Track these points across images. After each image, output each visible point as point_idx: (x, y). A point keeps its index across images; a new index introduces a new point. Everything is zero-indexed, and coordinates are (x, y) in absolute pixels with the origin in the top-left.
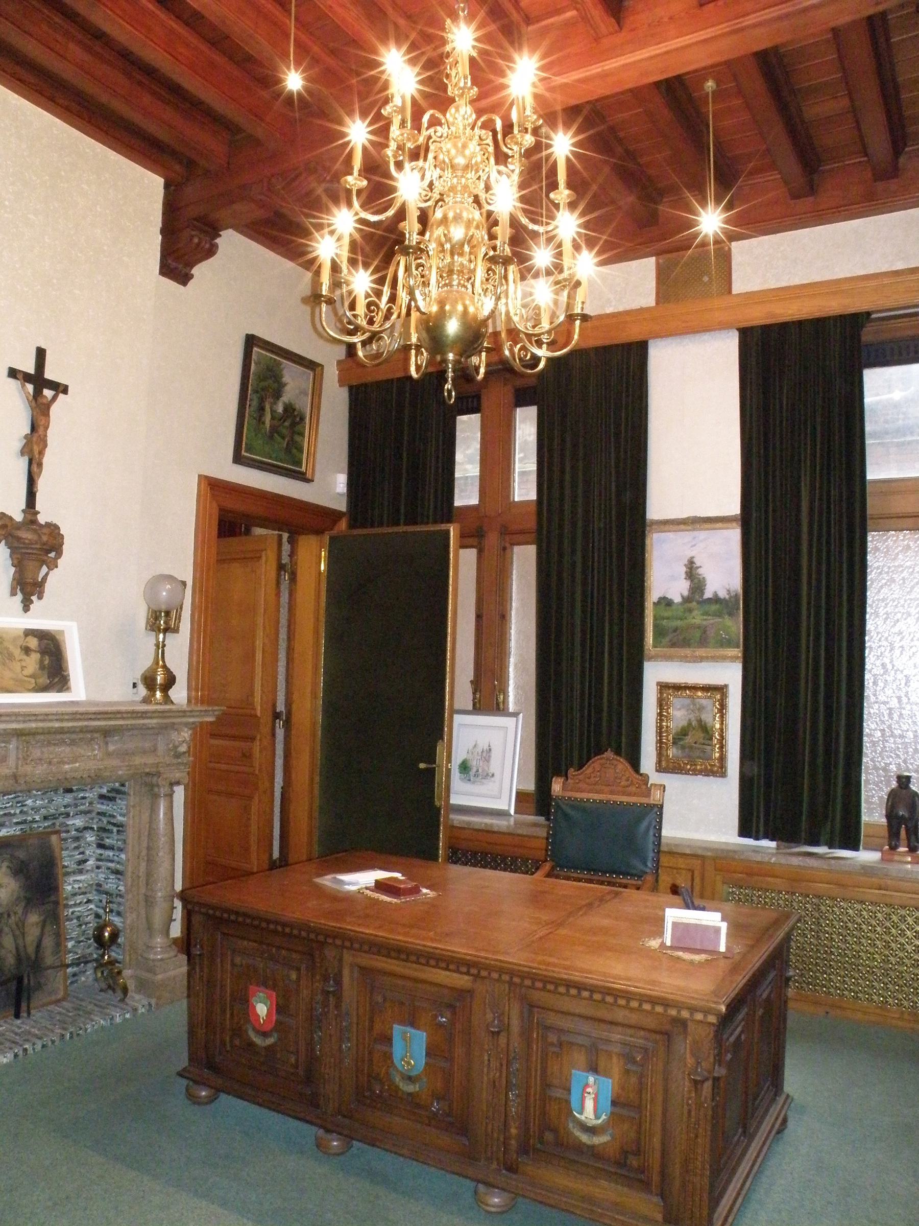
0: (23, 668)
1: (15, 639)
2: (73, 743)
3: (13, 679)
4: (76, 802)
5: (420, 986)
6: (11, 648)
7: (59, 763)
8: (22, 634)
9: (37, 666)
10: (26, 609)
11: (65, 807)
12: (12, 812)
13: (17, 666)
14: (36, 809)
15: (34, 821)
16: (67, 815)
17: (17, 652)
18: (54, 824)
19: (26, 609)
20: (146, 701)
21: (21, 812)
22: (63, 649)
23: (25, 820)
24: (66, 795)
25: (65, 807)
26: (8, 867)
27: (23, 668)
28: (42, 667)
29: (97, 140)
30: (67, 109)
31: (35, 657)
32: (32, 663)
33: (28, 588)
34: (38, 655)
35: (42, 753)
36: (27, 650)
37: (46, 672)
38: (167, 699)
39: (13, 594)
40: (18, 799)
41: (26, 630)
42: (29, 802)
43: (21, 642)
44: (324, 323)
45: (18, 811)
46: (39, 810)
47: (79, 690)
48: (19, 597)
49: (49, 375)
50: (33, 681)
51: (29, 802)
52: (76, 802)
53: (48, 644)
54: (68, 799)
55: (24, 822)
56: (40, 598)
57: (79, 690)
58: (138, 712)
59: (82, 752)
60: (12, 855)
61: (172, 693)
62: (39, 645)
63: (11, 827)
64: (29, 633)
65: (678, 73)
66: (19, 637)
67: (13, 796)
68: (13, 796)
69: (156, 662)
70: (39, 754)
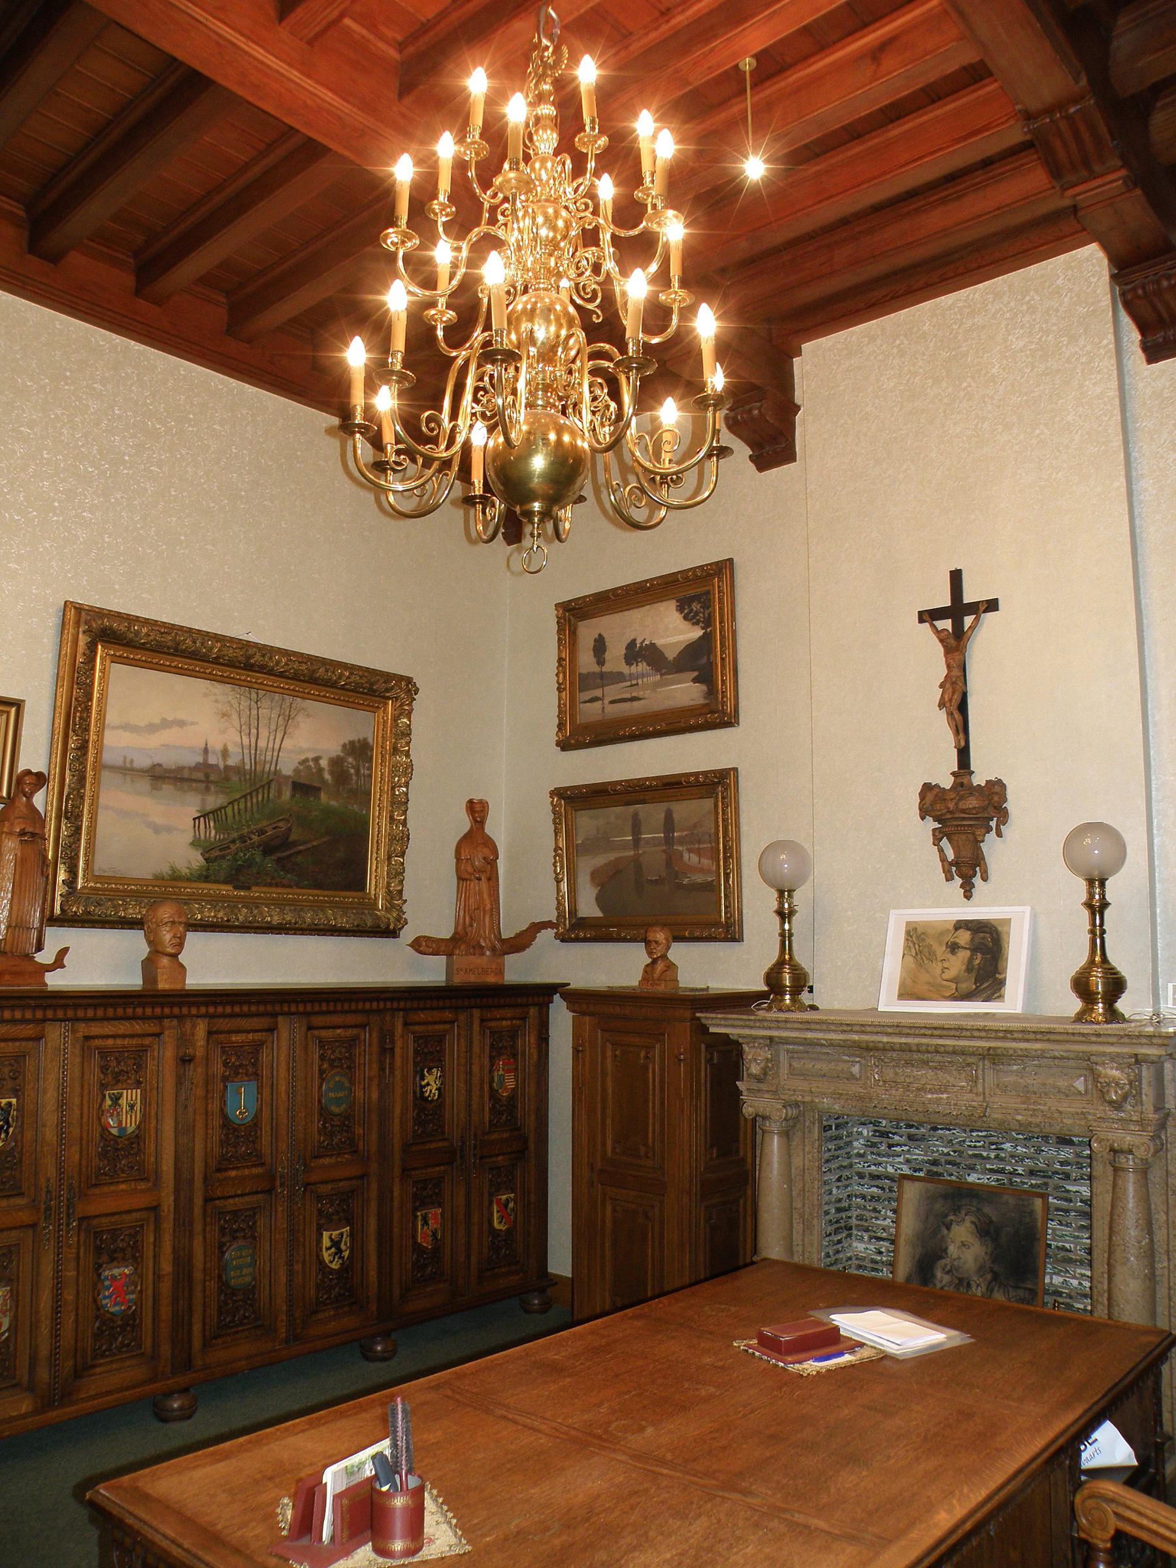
0: (944, 970)
1: (942, 934)
2: (941, 1067)
3: (929, 983)
4: (1080, 1160)
5: (965, 1550)
6: (935, 947)
7: (918, 1089)
8: (951, 927)
9: (964, 967)
10: (968, 895)
11: (1062, 1164)
12: (985, 1154)
13: (937, 968)
14: (1021, 1159)
15: (1014, 1173)
16: (1067, 1176)
17: (940, 950)
18: (1046, 1184)
19: (968, 895)
20: (1079, 1018)
21: (997, 1157)
22: (1004, 944)
23: (1003, 1169)
24: (1062, 1147)
25: (1062, 1164)
26: (972, 1222)
27: (944, 970)
28: (969, 969)
29: (876, 318)
30: (927, 286)
31: (964, 955)
32: (957, 964)
33: (967, 868)
34: (968, 953)
35: (896, 1074)
36: (954, 948)
37: (974, 974)
38: (1113, 1015)
39: (949, 878)
40: (994, 1139)
41: (959, 921)
42: (1007, 1146)
43: (949, 938)
44: (712, 486)
45: (992, 1155)
46: (1022, 1160)
47: (1013, 1002)
48: (958, 881)
49: (945, 601)
50: (954, 986)
51: (1007, 1146)
52: (1080, 1160)
53: (984, 938)
54: (1067, 1153)
55: (1001, 1171)
56: (985, 878)
57: (1013, 1002)
58: (997, 1031)
59: (952, 1080)
60: (979, 1210)
61: (1122, 1005)
62: (972, 939)
63: (983, 1173)
64: (960, 925)
65: (213, 77)
66: (948, 930)
67: (984, 1134)
68: (984, 1134)
69: (1091, 962)
70: (892, 1075)
